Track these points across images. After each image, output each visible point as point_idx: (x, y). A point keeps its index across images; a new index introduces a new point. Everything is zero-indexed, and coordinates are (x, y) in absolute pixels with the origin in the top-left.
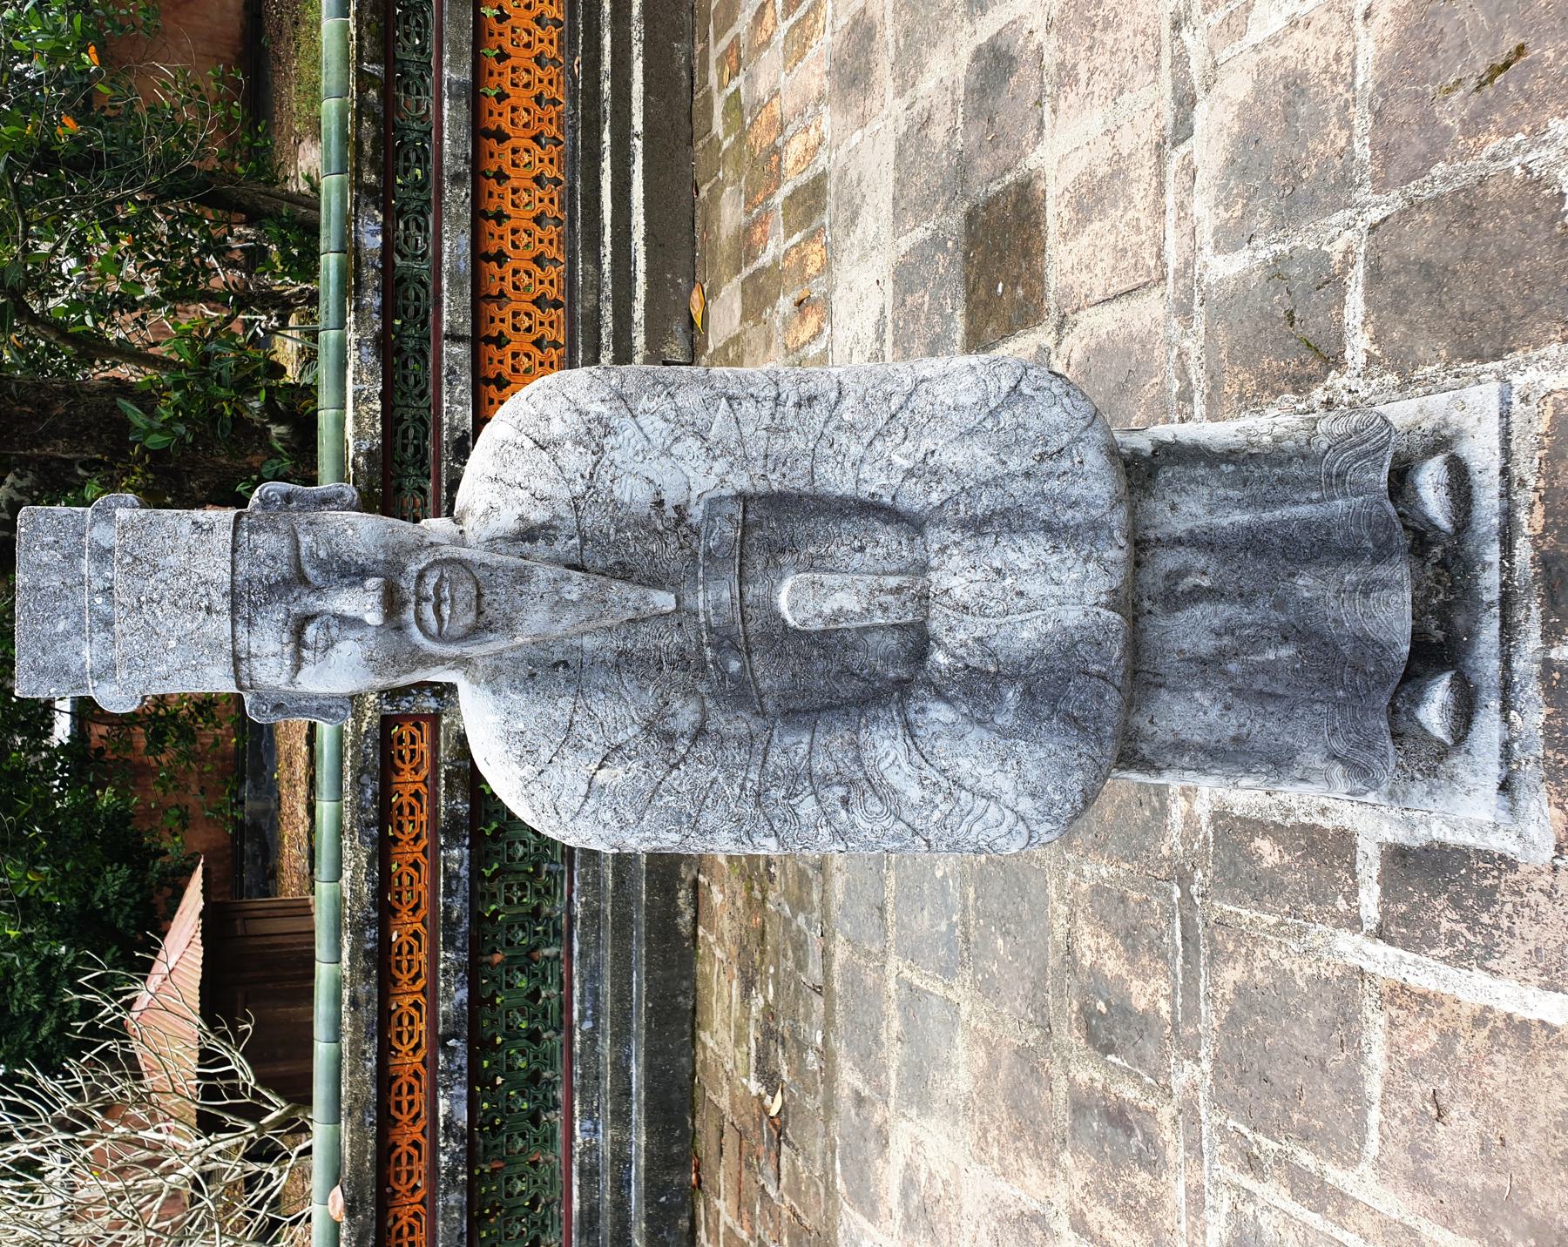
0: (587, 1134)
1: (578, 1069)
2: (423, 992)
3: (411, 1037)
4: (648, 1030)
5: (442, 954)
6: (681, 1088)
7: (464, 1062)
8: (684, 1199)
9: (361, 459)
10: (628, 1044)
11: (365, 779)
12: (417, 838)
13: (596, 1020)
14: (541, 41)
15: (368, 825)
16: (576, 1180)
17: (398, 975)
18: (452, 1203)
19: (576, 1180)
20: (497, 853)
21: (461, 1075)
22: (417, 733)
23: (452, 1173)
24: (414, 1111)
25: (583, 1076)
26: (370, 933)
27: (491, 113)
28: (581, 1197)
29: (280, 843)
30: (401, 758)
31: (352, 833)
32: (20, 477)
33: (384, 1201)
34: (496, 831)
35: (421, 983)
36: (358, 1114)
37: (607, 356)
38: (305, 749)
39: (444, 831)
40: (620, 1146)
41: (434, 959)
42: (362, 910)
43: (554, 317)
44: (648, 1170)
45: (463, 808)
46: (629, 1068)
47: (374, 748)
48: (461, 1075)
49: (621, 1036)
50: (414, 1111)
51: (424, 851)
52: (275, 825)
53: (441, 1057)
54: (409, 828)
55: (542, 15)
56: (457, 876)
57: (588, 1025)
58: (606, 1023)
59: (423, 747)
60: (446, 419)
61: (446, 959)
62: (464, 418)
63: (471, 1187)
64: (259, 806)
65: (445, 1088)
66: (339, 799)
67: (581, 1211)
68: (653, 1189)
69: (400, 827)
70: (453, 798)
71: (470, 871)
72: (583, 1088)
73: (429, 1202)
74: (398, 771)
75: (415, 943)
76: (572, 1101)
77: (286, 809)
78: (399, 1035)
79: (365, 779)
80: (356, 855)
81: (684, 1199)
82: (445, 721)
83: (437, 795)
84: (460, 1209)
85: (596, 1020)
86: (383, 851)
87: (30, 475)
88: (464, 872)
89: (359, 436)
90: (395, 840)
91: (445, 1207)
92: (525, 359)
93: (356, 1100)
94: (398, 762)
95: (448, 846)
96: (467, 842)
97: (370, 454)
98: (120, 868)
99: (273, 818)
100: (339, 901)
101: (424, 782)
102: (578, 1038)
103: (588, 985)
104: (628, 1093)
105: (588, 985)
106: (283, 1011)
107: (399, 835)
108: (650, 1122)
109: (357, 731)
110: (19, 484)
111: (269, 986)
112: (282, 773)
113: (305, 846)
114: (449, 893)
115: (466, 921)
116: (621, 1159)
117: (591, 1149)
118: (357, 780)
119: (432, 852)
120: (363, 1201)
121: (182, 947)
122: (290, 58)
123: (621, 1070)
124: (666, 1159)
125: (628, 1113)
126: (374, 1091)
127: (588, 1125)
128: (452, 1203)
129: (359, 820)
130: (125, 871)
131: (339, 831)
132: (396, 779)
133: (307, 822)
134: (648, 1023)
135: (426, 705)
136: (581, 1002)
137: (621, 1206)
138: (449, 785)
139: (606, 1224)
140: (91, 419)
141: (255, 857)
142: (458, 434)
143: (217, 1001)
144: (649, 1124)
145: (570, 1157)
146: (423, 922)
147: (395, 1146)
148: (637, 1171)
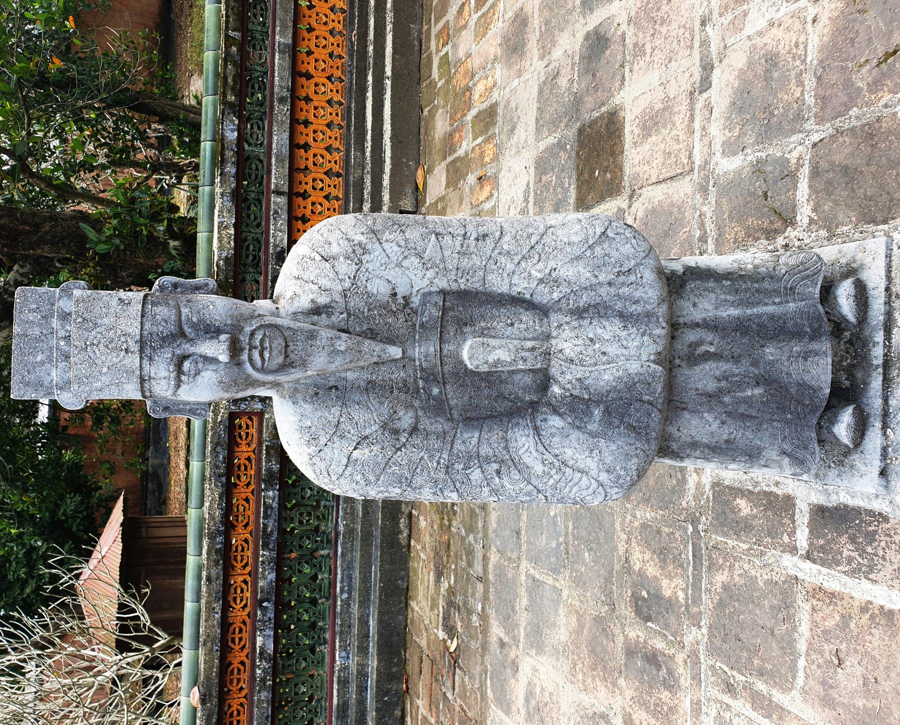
1: (338, 621)
2: (249, 574)
4: (380, 600)
5: (261, 552)
6: (398, 634)
7: (272, 616)
8: (399, 699)
9: (221, 262)
10: (368, 607)
11: (219, 449)
12: (248, 484)
14: (333, 21)
15: (220, 476)
16: (335, 686)
18: (263, 698)
19: (335, 686)
20: (295, 494)
22: (250, 423)
23: (263, 680)
24: (242, 643)
25: (341, 626)
26: (220, 539)
27: (303, 87)
28: (338, 696)
29: (169, 484)
30: (236, 560)
31: (210, 480)
32: (22, 267)
34: (295, 482)
35: (248, 569)
36: (209, 644)
37: (367, 206)
38: (185, 429)
39: (264, 481)
41: (256, 555)
42: (215, 525)
43: (337, 182)
45: (276, 467)
46: (368, 621)
47: (224, 431)
48: (270, 623)
49: (364, 603)
51: (252, 492)
52: (167, 473)
54: (243, 478)
55: (332, 75)
56: (271, 507)
57: (345, 596)
58: (356, 595)
59: (253, 431)
60: (272, 240)
61: (263, 555)
62: (282, 240)
63: (274, 689)
64: (157, 462)
65: (261, 630)
66: (203, 460)
67: (338, 704)
68: (381, 692)
69: (239, 477)
70: (270, 461)
71: (279, 504)
72: (341, 633)
73: (249, 697)
74: (238, 445)
75: (245, 545)
77: (173, 464)
78: (235, 599)
79: (219, 449)
80: (212, 493)
81: (399, 699)
82: (266, 416)
83: (260, 459)
84: (268, 701)
85: (350, 593)
86: (228, 491)
87: (28, 265)
88: (275, 505)
89: (221, 248)
90: (235, 485)
91: (259, 700)
93: (208, 636)
94: (239, 440)
95: (266, 490)
96: (277, 487)
97: (227, 259)
98: (75, 496)
99: (165, 469)
100: (202, 520)
101: (253, 451)
102: (339, 603)
103: (346, 572)
105: (346, 572)
106: (168, 582)
107: (238, 482)
108: (379, 654)
109: (215, 421)
110: (21, 271)
112: (171, 443)
113: (184, 486)
114: (266, 517)
115: (276, 533)
116: (362, 674)
117: (345, 668)
118: (214, 449)
119: (257, 493)
120: (211, 696)
121: (110, 543)
122: (187, 27)
123: (364, 622)
125: (367, 648)
126: (219, 631)
127: (344, 654)
128: (263, 698)
129: (215, 473)
130: (78, 498)
131: (203, 479)
132: (237, 449)
133: (185, 473)
134: (380, 595)
135: (255, 406)
136: (342, 582)
137: (361, 702)
138: (268, 454)
139: (352, 712)
140: (65, 234)
141: (154, 491)
142: (279, 249)
143: (129, 575)
145: (332, 673)
146: (252, 492)
147: (230, 664)
148: (372, 682)
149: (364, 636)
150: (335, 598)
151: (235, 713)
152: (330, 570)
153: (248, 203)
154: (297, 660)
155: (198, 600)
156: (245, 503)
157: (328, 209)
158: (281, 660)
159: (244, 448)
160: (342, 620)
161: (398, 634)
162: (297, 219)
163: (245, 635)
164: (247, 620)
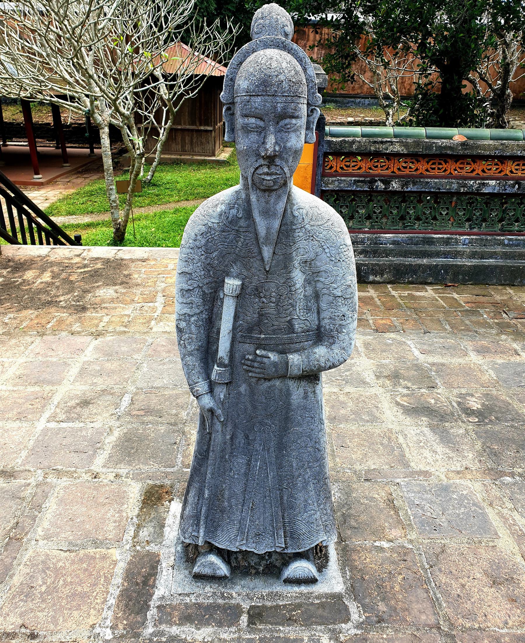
0: (464, 241)
2: (336, 171)
3: (347, 166)
4: (511, 267)
6: (484, 280)
7: (507, 191)
8: (440, 280)
10: (502, 258)
13: (507, 245)
17: (458, 163)
19: (445, 236)
21: (503, 190)
23: (465, 186)
24: (345, 168)
25: (487, 239)
28: (439, 238)
30: (433, 164)
33: (457, 158)
35: (340, 171)
36: (501, 147)
40: (457, 254)
44: (456, 266)
48: (503, 190)
49: (506, 256)
50: (345, 168)
53: (512, 182)
57: (506, 242)
58: (508, 250)
63: (458, 193)
65: (499, 183)
67: (433, 238)
68: (447, 268)
72: (482, 240)
73: (450, 176)
75: (356, 168)
76: (474, 235)
78: (518, 165)
81: (440, 280)
84: (450, 189)
85: (507, 245)
91: (452, 183)
92: (445, 213)
94: (516, 163)
102: (502, 238)
103: (522, 242)
104: (455, 257)
105: (522, 242)
116: (457, 254)
117: (457, 242)
120: (466, 149)
123: (492, 255)
124: (458, 273)
125: (474, 258)
126: (508, 154)
127: (467, 241)
134: (514, 267)
136: (516, 240)
137: (438, 254)
139: (427, 248)
144: (474, 266)
147: (446, 162)
148: (450, 261)
151: (441, 166)
152: (520, 231)
154: (464, 209)
155: (363, 136)
157: (393, 218)
158: (472, 197)
159: (426, 166)
160: (490, 240)
163: (436, 172)
164: (502, 174)
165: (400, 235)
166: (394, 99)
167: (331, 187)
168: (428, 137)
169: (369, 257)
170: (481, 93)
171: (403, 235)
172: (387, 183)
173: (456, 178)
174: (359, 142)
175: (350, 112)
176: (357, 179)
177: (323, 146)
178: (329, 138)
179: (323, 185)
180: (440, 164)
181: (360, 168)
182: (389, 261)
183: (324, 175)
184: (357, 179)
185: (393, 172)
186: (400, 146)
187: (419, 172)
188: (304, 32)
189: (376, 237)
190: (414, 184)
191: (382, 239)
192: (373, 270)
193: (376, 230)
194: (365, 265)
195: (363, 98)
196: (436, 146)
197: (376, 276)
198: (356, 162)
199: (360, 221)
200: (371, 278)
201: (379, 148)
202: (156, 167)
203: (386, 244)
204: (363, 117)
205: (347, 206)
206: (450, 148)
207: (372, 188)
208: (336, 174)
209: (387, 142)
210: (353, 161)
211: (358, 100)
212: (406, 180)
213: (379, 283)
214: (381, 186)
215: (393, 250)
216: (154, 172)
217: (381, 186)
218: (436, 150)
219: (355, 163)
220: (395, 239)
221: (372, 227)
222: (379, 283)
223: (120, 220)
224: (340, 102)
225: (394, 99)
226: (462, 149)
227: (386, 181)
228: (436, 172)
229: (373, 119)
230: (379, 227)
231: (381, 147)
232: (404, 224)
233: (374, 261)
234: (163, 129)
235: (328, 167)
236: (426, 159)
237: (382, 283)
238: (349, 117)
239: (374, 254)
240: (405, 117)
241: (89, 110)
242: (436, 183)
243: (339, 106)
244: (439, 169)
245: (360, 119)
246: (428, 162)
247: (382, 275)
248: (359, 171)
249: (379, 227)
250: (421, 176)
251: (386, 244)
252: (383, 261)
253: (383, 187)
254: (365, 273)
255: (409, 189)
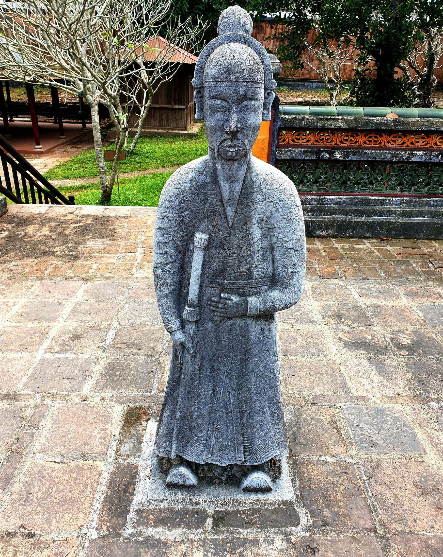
0: (396, 202)
1: (417, 199)
2: (288, 143)
4: (436, 224)
6: (413, 234)
7: (433, 161)
8: (376, 235)
10: (428, 217)
13: (433, 206)
16: (380, 198)
18: (387, 155)
19: (380, 198)
23: (397, 156)
24: (296, 141)
25: (415, 201)
28: (375, 199)
30: (370, 137)
35: (292, 143)
36: (427, 124)
37: (37, 201)
40: (390, 213)
46: (420, 217)
49: (431, 215)
57: (432, 203)
58: (433, 209)
65: (426, 154)
67: (370, 199)
68: (381, 224)
72: (411, 201)
73: (384, 148)
75: (305, 140)
81: (376, 235)
84: (384, 158)
85: (433, 206)
91: (386, 153)
93: (432, 123)
102: (428, 200)
108: (405, 223)
111: (173, 87)
116: (390, 213)
117: (390, 203)
120: (397, 125)
123: (420, 214)
125: (405, 216)
126: (433, 129)
127: (399, 202)
128: (387, 155)
134: (438, 224)
136: (440, 201)
137: (374, 213)
139: (365, 207)
145: (386, 196)
147: (381, 136)
148: (385, 219)
149: (412, 215)
150: (429, 197)
151: (376, 139)
153: (403, 137)
154: (396, 176)
155: (311, 114)
156: (307, 139)
157: (336, 183)
159: (364, 139)
160: (418, 201)
161: (413, 234)
162: (359, 164)
163: (372, 144)
164: (428, 146)
165: (342, 197)
166: (337, 83)
167: (284, 156)
168: (365, 115)
169: (316, 215)
170: (410, 78)
171: (345, 197)
172: (331, 153)
173: (389, 149)
174: (308, 119)
175: (300, 93)
176: (306, 150)
177: (277, 122)
178: (283, 116)
179: (278, 155)
180: (376, 137)
181: (308, 141)
182: (333, 218)
183: (278, 147)
184: (306, 150)
185: (336, 144)
186: (342, 122)
187: (358, 144)
188: (262, 27)
189: (322, 199)
190: (354, 154)
191: (326, 200)
192: (319, 226)
193: (322, 192)
194: (312, 222)
195: (311, 82)
196: (372, 123)
197: (322, 231)
198: (305, 135)
199: (308, 185)
200: (318, 233)
201: (324, 124)
202: (138, 139)
203: (330, 204)
204: (312, 98)
205: (297, 173)
206: (385, 124)
207: (319, 157)
208: (288, 146)
209: (331, 119)
210: (303, 135)
211: (307, 84)
212: (348, 151)
213: (324, 237)
214: (326, 156)
215: (336, 209)
216: (136, 144)
217: (326, 156)
218: (372, 126)
219: (304, 137)
220: (338, 200)
221: (319, 190)
222: (324, 237)
223: (107, 183)
224: (291, 85)
225: (337, 83)
226: (394, 125)
227: (330, 151)
228: (372, 144)
229: (319, 99)
230: (324, 190)
231: (326, 123)
232: (345, 187)
233: (320, 218)
234: (143, 107)
235: (282, 140)
236: (364, 134)
237: (327, 237)
238: (299, 97)
239: (320, 212)
240: (347, 98)
241: (82, 92)
242: (372, 153)
243: (291, 89)
244: (375, 141)
245: (308, 99)
246: (365, 136)
247: (327, 230)
248: (307, 143)
249: (324, 190)
250: (360, 147)
251: (330, 204)
252: (328, 218)
253: (328, 156)
254: (313, 229)
255: (350, 158)
